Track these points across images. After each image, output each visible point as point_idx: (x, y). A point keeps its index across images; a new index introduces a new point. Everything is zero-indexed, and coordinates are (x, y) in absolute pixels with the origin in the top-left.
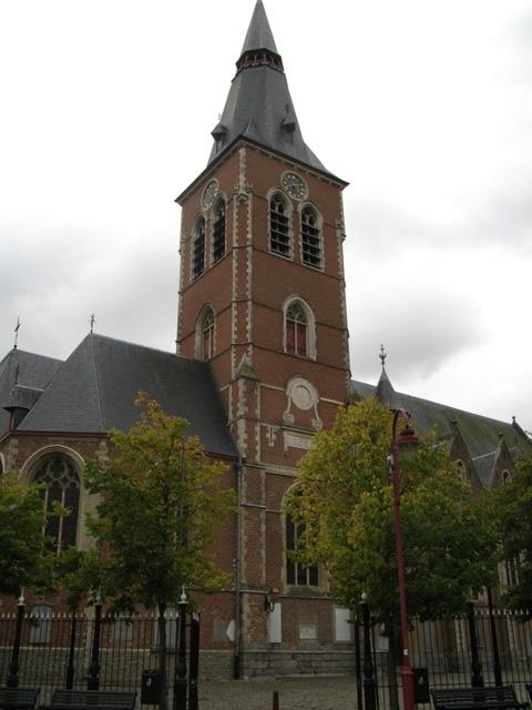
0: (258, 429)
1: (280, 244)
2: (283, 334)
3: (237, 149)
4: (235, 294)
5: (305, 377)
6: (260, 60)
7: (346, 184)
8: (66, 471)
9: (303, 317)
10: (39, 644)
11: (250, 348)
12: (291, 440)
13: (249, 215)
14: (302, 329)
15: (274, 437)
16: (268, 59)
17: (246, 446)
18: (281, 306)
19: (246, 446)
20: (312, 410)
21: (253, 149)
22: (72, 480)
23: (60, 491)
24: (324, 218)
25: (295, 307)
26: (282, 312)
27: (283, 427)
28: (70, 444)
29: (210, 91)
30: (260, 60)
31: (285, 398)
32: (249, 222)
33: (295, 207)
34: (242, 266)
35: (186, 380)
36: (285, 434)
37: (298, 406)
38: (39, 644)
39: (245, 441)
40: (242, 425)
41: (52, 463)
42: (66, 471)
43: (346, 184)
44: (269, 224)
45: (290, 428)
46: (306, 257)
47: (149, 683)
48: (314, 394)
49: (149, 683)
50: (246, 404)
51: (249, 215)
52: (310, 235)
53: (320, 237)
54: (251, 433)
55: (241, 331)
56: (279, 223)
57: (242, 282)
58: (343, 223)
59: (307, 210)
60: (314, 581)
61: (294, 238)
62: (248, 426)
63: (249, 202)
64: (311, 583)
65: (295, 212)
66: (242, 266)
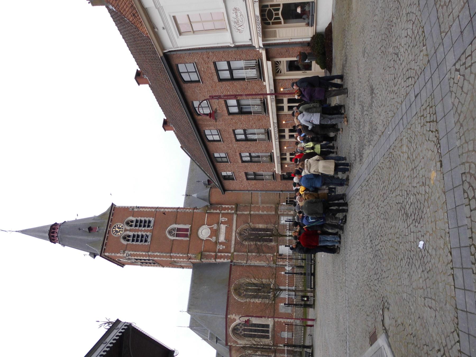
0: (219, 254)
1: (143, 239)
2: (182, 240)
3: (106, 256)
4: (168, 259)
5: (198, 230)
6: (54, 233)
7: (113, 204)
8: (238, 327)
9: (174, 229)
10: (293, 335)
11: (189, 255)
12: (222, 238)
13: (135, 253)
14: (179, 230)
15: (221, 246)
16: (53, 233)
17: (226, 259)
18: (171, 240)
19: (226, 259)
20: (210, 228)
21: (105, 249)
22: (241, 325)
23: (245, 334)
24: (130, 216)
25: (170, 232)
26: (173, 240)
27: (216, 243)
28: (229, 327)
29: (75, 258)
30: (54, 233)
31: (207, 240)
32: (138, 253)
33: (128, 230)
34: (157, 256)
35: (201, 274)
36: (220, 241)
37: (209, 235)
38: (293, 335)
39: (224, 259)
40: (218, 260)
41: (235, 331)
42: (238, 327)
43: (113, 204)
44: (137, 243)
45: (217, 238)
46: (149, 226)
47: (333, 190)
48: (204, 226)
49: (333, 190)
50: (211, 259)
51: (135, 253)
52: (139, 224)
53: (139, 219)
54: (221, 257)
55: (183, 258)
56: (136, 238)
57: (163, 257)
58: (131, 207)
59: (127, 223)
60: (267, 326)
61: (142, 231)
62: (218, 258)
63: (129, 253)
64: (269, 333)
65: (130, 230)
66: (157, 256)
